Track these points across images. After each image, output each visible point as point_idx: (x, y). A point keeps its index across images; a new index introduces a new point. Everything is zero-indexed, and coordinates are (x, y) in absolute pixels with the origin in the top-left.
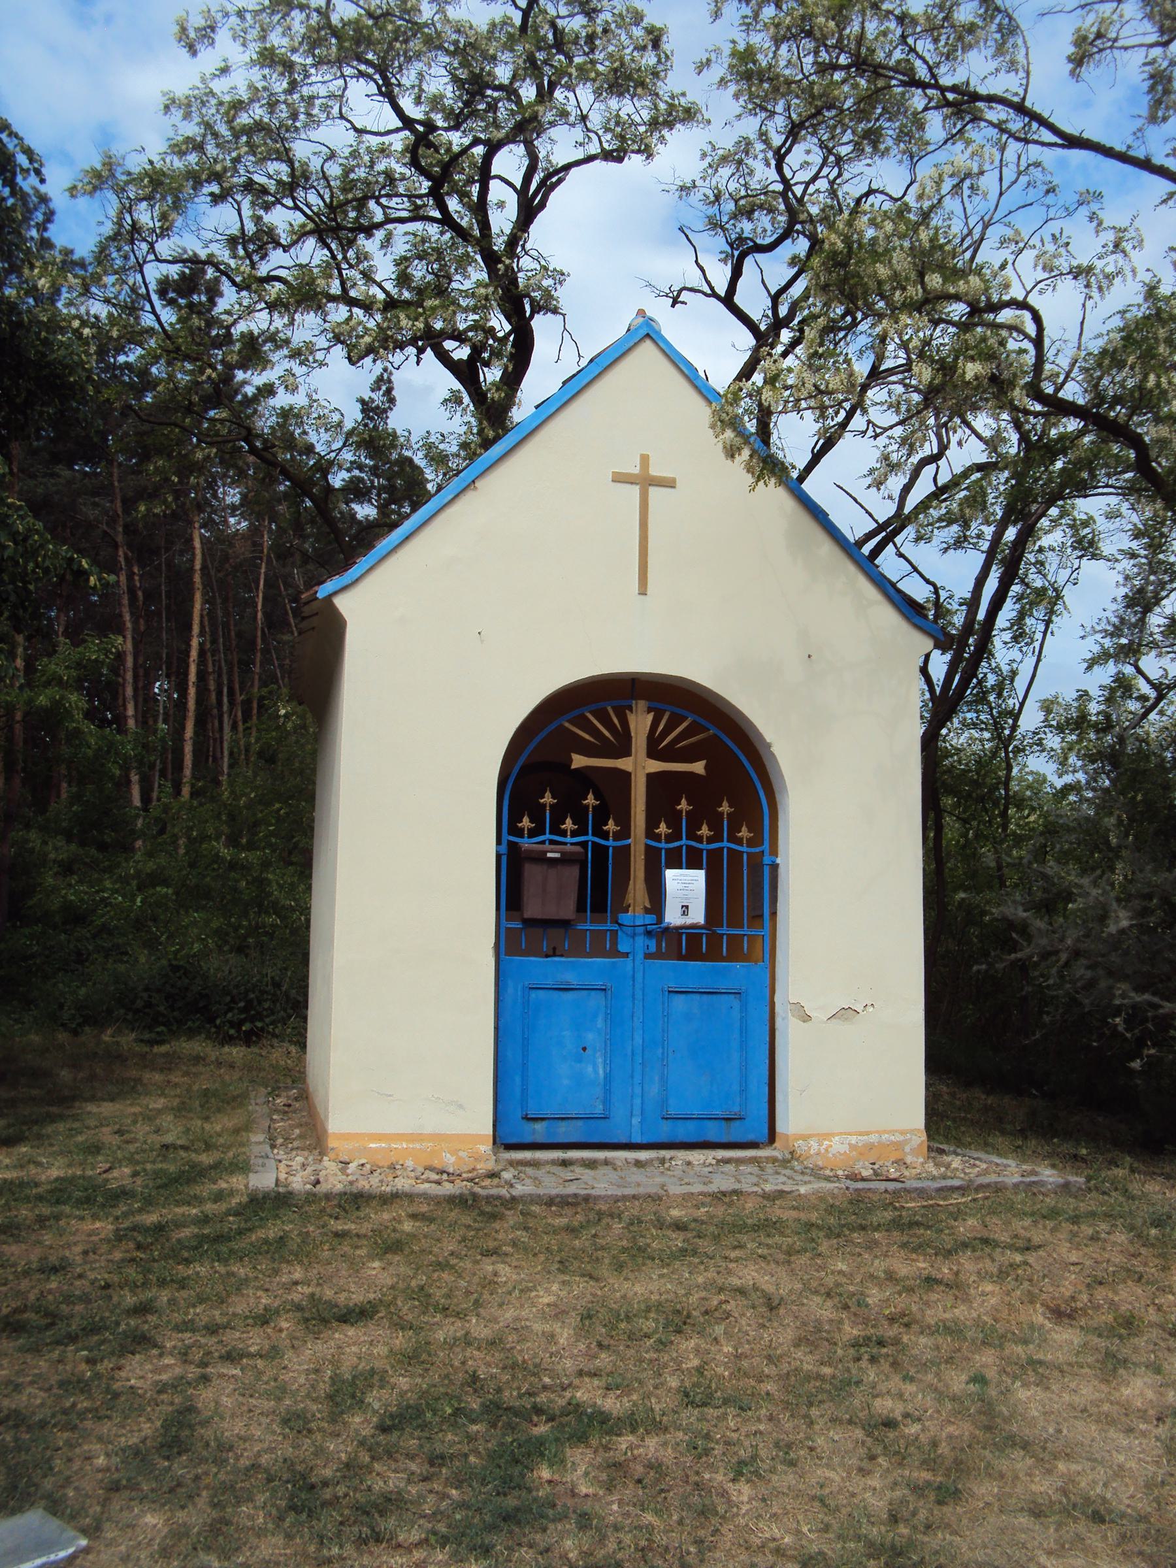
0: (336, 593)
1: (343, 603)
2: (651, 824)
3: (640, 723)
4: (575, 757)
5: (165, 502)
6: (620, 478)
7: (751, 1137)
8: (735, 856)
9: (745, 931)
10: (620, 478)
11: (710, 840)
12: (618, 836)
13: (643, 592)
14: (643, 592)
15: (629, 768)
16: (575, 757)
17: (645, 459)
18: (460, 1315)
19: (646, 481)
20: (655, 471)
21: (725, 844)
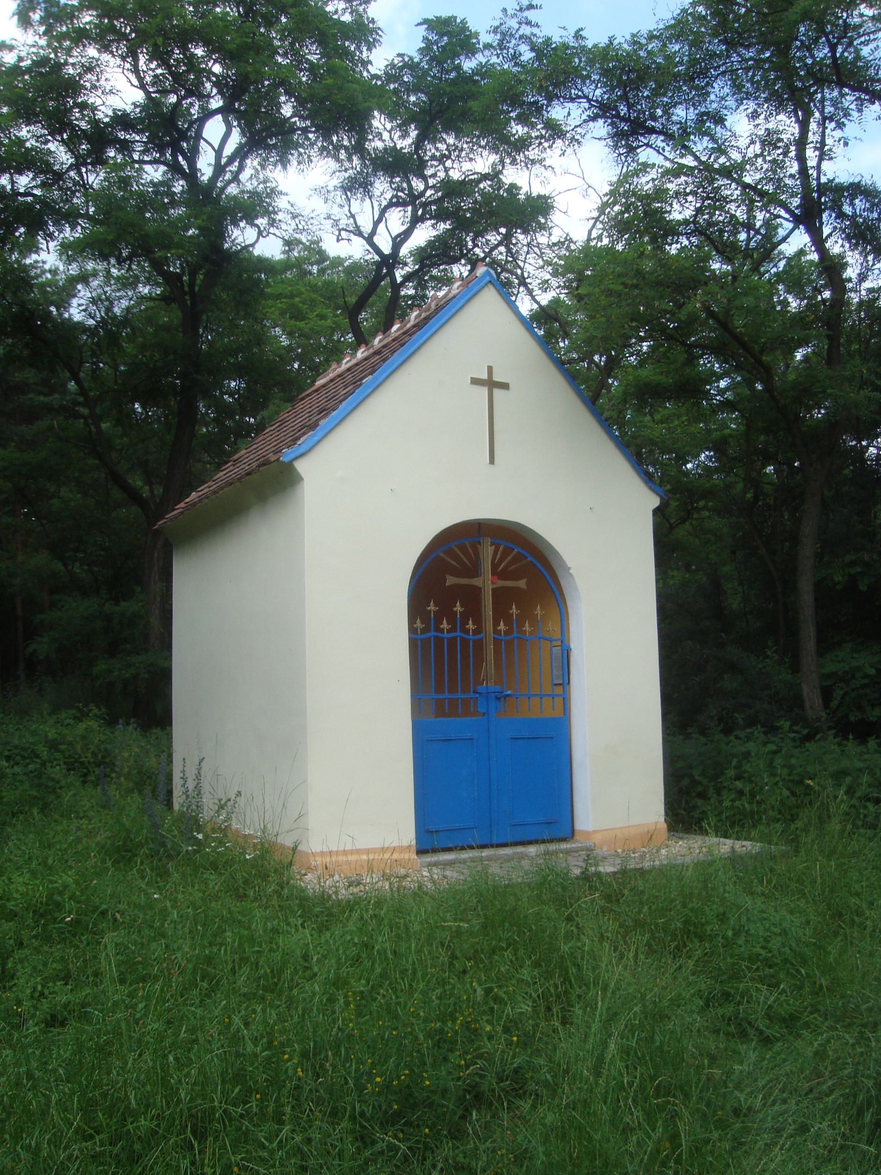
0: (296, 458)
1: (301, 466)
2: (496, 624)
3: (487, 552)
4: (448, 577)
5: (231, 395)
6: (475, 381)
7: (562, 835)
8: (465, 642)
9: (459, 695)
10: (475, 381)
11: (449, 631)
12: (476, 632)
13: (492, 461)
14: (492, 461)
15: (481, 585)
16: (448, 577)
17: (490, 369)
18: (48, 1105)
19: (491, 384)
20: (496, 378)
21: (458, 633)
